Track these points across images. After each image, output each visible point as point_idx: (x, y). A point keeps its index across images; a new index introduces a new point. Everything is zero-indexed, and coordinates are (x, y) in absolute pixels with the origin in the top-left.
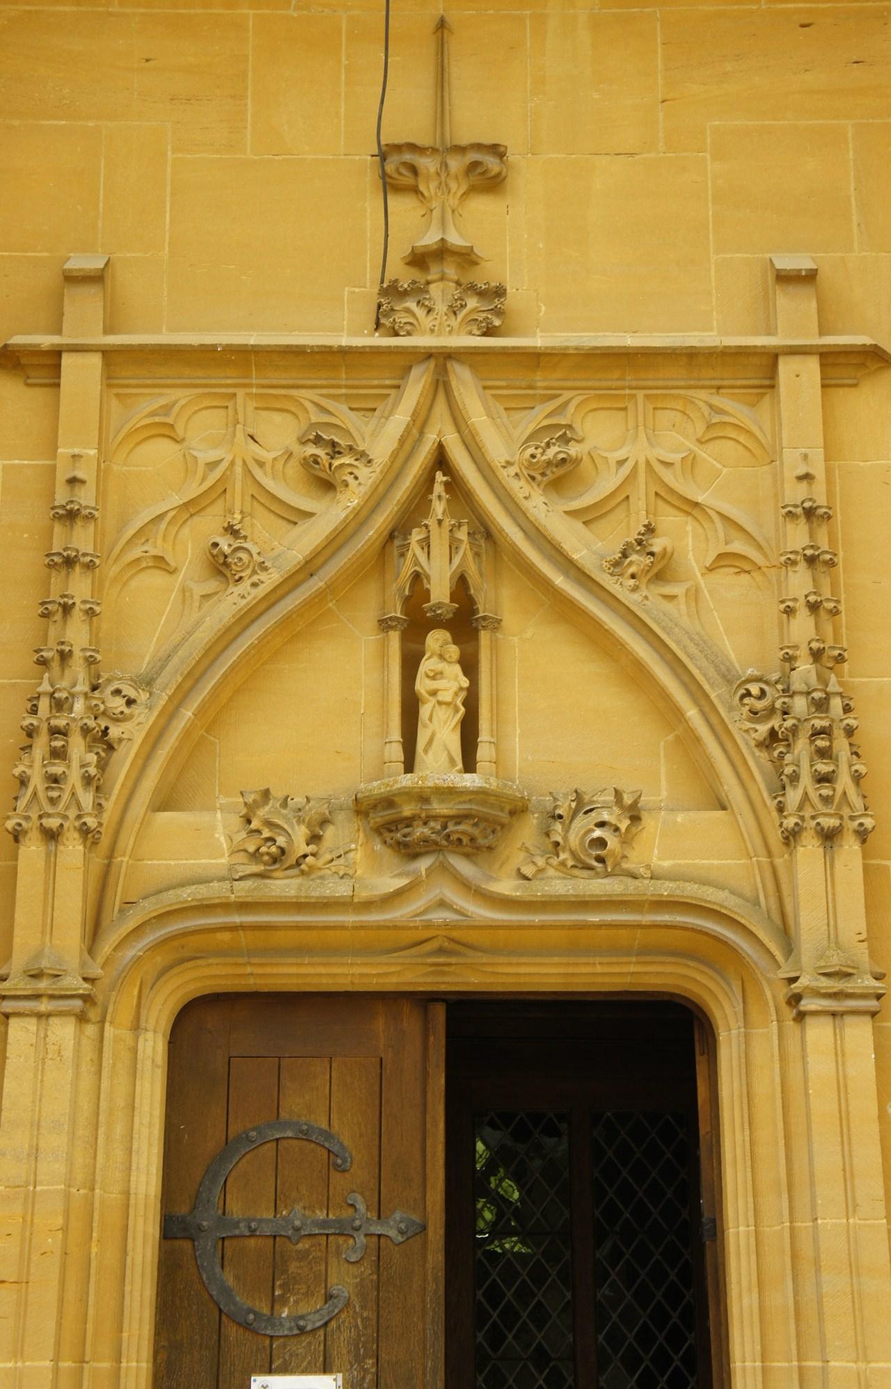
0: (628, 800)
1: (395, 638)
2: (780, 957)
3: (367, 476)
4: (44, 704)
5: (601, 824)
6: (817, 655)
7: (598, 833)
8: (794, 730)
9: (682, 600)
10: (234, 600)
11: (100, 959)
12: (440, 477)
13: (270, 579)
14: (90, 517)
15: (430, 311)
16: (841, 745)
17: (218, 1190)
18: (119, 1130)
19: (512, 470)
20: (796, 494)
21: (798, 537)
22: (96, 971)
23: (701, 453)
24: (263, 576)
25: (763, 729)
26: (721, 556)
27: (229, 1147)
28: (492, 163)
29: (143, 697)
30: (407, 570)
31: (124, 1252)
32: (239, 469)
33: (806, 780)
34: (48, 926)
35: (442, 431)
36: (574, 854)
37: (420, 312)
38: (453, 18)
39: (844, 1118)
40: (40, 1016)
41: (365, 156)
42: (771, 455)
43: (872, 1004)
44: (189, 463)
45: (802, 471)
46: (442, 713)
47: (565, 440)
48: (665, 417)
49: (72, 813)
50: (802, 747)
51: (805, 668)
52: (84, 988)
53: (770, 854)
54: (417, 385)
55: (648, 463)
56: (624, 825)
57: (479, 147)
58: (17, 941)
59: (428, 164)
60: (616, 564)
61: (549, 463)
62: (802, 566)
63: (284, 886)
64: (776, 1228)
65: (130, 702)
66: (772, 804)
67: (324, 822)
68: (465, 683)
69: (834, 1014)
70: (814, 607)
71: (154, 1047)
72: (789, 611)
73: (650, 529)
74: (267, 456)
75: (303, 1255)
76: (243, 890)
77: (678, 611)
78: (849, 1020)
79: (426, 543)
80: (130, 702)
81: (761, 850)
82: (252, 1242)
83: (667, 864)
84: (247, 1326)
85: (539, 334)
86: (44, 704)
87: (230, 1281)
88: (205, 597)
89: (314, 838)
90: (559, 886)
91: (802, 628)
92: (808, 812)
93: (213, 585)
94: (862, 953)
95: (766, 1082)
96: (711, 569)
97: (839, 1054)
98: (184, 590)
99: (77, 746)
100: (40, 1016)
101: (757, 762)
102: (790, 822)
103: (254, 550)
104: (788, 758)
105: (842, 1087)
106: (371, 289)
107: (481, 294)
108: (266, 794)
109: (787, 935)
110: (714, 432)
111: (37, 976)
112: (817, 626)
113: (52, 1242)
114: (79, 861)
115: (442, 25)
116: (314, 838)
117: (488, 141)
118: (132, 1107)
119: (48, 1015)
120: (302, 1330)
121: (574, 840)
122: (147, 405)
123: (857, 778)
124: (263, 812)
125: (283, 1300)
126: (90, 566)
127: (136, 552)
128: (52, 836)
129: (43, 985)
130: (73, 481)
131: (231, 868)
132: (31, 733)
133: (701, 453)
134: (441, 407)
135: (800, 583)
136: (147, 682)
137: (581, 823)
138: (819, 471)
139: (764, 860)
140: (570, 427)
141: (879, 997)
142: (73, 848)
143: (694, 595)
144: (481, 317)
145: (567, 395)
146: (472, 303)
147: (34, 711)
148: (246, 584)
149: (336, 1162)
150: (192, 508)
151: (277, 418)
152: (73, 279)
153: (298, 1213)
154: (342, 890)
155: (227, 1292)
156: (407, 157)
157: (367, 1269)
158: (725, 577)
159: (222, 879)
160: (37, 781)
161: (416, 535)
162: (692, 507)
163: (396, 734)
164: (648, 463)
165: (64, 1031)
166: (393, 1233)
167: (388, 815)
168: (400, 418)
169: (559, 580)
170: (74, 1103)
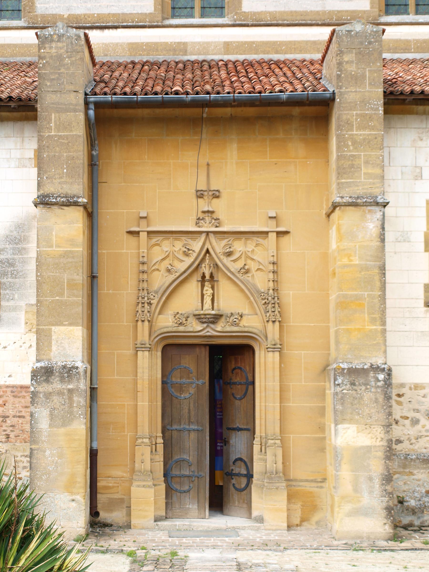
0: (240, 314)
1: (200, 284)
2: (265, 340)
3: (195, 255)
4: (140, 298)
5: (236, 318)
6: (273, 290)
7: (235, 320)
8: (269, 303)
9: (251, 277)
10: (172, 277)
11: (151, 341)
12: (208, 255)
13: (178, 274)
14: (146, 263)
15: (206, 223)
16: (277, 306)
17: (171, 376)
18: (155, 367)
19: (221, 254)
20: (271, 259)
21: (271, 267)
22: (151, 343)
23: (255, 249)
24: (176, 274)
25: (264, 301)
26: (258, 269)
27: (173, 370)
28: (217, 193)
29: (156, 295)
30: (202, 272)
31: (157, 387)
32: (171, 252)
33: (270, 312)
34: (143, 336)
35: (208, 246)
36: (231, 323)
37: (204, 223)
38: (210, 163)
39: (274, 368)
40: (142, 351)
41: (194, 191)
42: (267, 250)
43: (279, 350)
44: (162, 251)
45: (272, 255)
46: (208, 297)
47: (230, 247)
48: (249, 242)
49: (146, 317)
50: (270, 306)
51: (271, 291)
52: (150, 346)
53: (264, 323)
54: (204, 236)
55: (245, 251)
56: (240, 318)
57: (214, 190)
58: (138, 338)
59: (206, 193)
60: (239, 271)
61: (227, 252)
62: (271, 273)
63: (181, 328)
64: (263, 384)
65: (154, 296)
66: (265, 315)
67: (188, 317)
68: (212, 292)
69: (273, 351)
70: (273, 281)
71: (159, 354)
72: (269, 281)
73: (245, 265)
74: (177, 249)
75: (185, 387)
76: (175, 329)
77: (250, 279)
78: (275, 352)
79: (205, 267)
80: (154, 296)
81: (263, 322)
82: (177, 385)
83: (247, 325)
84: (176, 398)
85: (226, 226)
86: (140, 298)
87: (173, 391)
88: (166, 276)
89: (186, 320)
90: (228, 329)
91: (271, 284)
92: (270, 317)
93: (167, 274)
94: (278, 341)
95: (262, 360)
96: (256, 271)
97: (273, 358)
98: (162, 275)
99: (146, 305)
100: (142, 351)
101: (262, 307)
102: (267, 319)
103: (175, 269)
104: (268, 308)
105: (274, 363)
106: (195, 218)
107: (215, 220)
108: (178, 313)
109: (266, 337)
110: (257, 245)
111: (142, 344)
112: (274, 284)
113: (147, 386)
114: (148, 325)
115: (208, 165)
116: (186, 320)
117: (216, 189)
118: (157, 364)
119: (144, 351)
120: (185, 398)
121: (231, 321)
122: (154, 241)
123: (279, 312)
124: (178, 316)
125: (182, 394)
126: (146, 272)
127: (153, 268)
128: (143, 321)
129: (143, 346)
130: (143, 257)
131: (172, 325)
132: (138, 303)
133: (255, 249)
134: (208, 242)
135: (271, 276)
136: (156, 292)
137: (232, 318)
138: (275, 254)
139: (263, 324)
140: (231, 244)
141: (280, 348)
142: (146, 323)
143: (253, 276)
144: (215, 224)
145: (231, 238)
146: (213, 221)
147: (138, 298)
148: (174, 275)
149: (190, 372)
150: (163, 259)
151: (178, 242)
152: (141, 218)
153: (184, 380)
154: (191, 330)
155: (172, 392)
156: (202, 192)
157: (196, 389)
158: (259, 272)
159: (171, 327)
160: (140, 312)
161: (203, 265)
162: (253, 259)
163: (200, 301)
164: (245, 251)
165: (147, 353)
166: (200, 384)
167: (199, 317)
168: (200, 244)
169: (229, 274)
170: (149, 365)
